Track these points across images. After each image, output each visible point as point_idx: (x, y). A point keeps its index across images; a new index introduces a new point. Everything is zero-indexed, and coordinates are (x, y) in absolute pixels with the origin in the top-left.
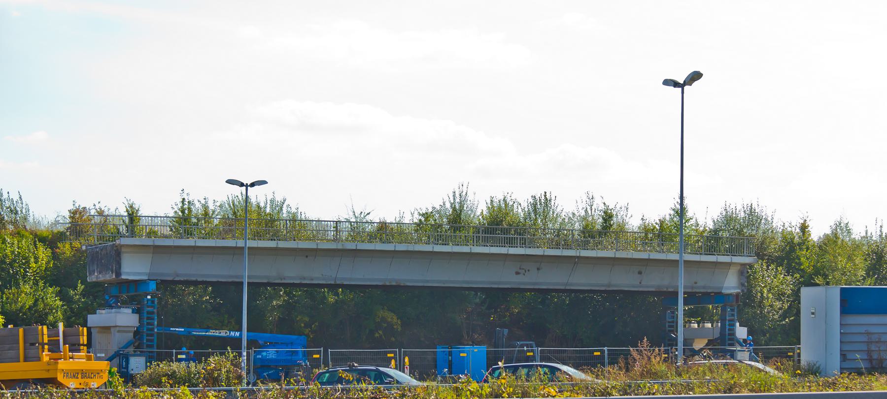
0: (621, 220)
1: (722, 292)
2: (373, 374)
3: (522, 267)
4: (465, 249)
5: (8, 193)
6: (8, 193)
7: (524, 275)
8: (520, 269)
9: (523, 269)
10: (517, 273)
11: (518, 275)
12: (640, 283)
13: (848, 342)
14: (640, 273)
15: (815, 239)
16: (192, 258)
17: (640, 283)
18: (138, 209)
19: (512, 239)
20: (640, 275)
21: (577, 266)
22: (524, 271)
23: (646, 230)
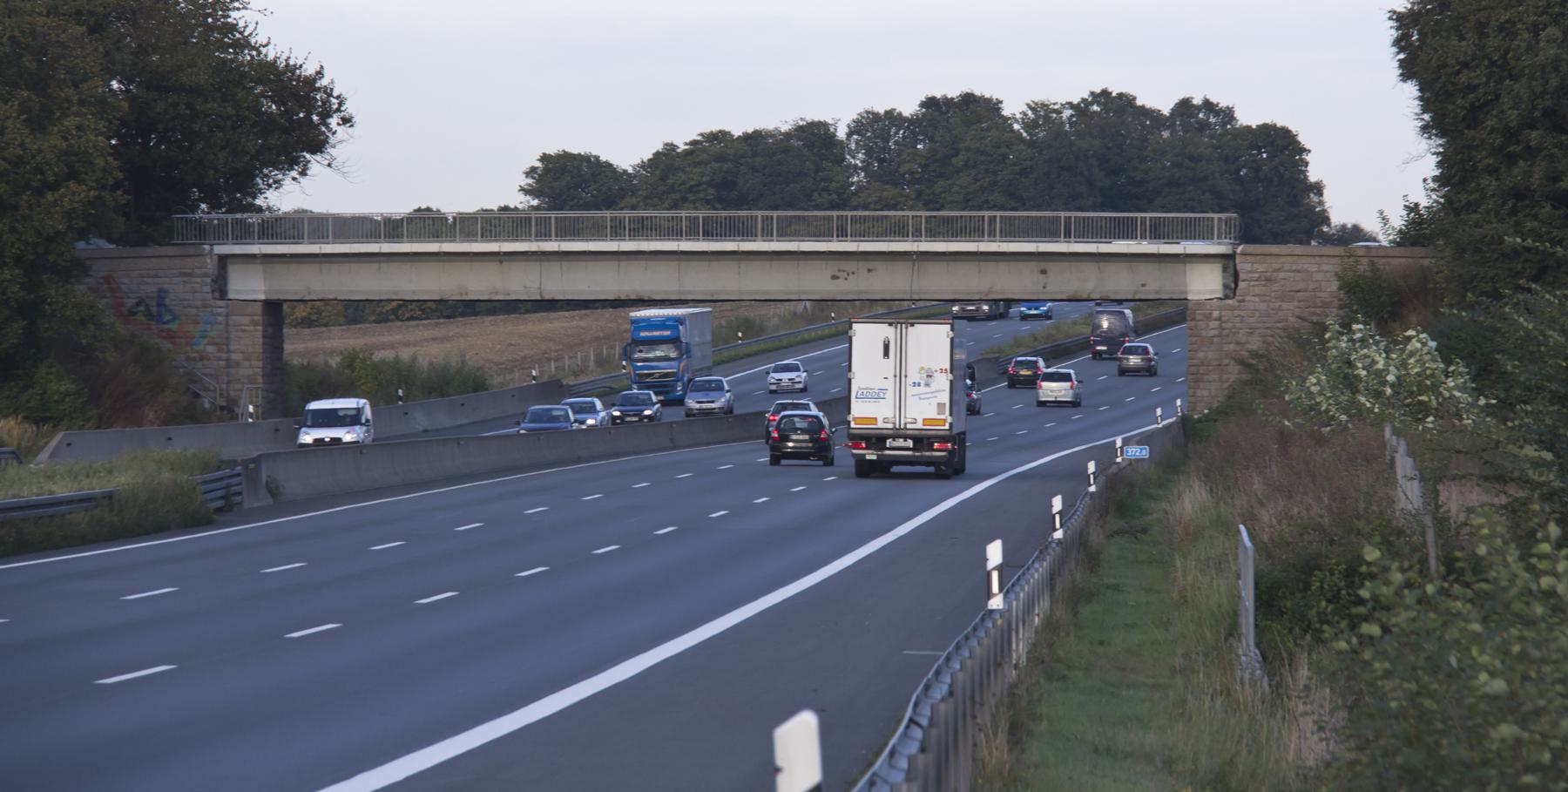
0: (251, 138)
1: (1189, 298)
2: (1140, 350)
3: (841, 268)
4: (493, 247)
5: (309, 53)
6: (257, 23)
7: (846, 279)
8: (839, 271)
9: (844, 271)
10: (835, 277)
11: (837, 281)
12: (1044, 287)
13: (693, 300)
14: (1044, 272)
15: (1168, 115)
16: (380, 268)
17: (1044, 287)
18: (1390, 12)
19: (545, 221)
20: (1042, 276)
21: (918, 268)
22: (845, 274)
23: (1143, 107)
